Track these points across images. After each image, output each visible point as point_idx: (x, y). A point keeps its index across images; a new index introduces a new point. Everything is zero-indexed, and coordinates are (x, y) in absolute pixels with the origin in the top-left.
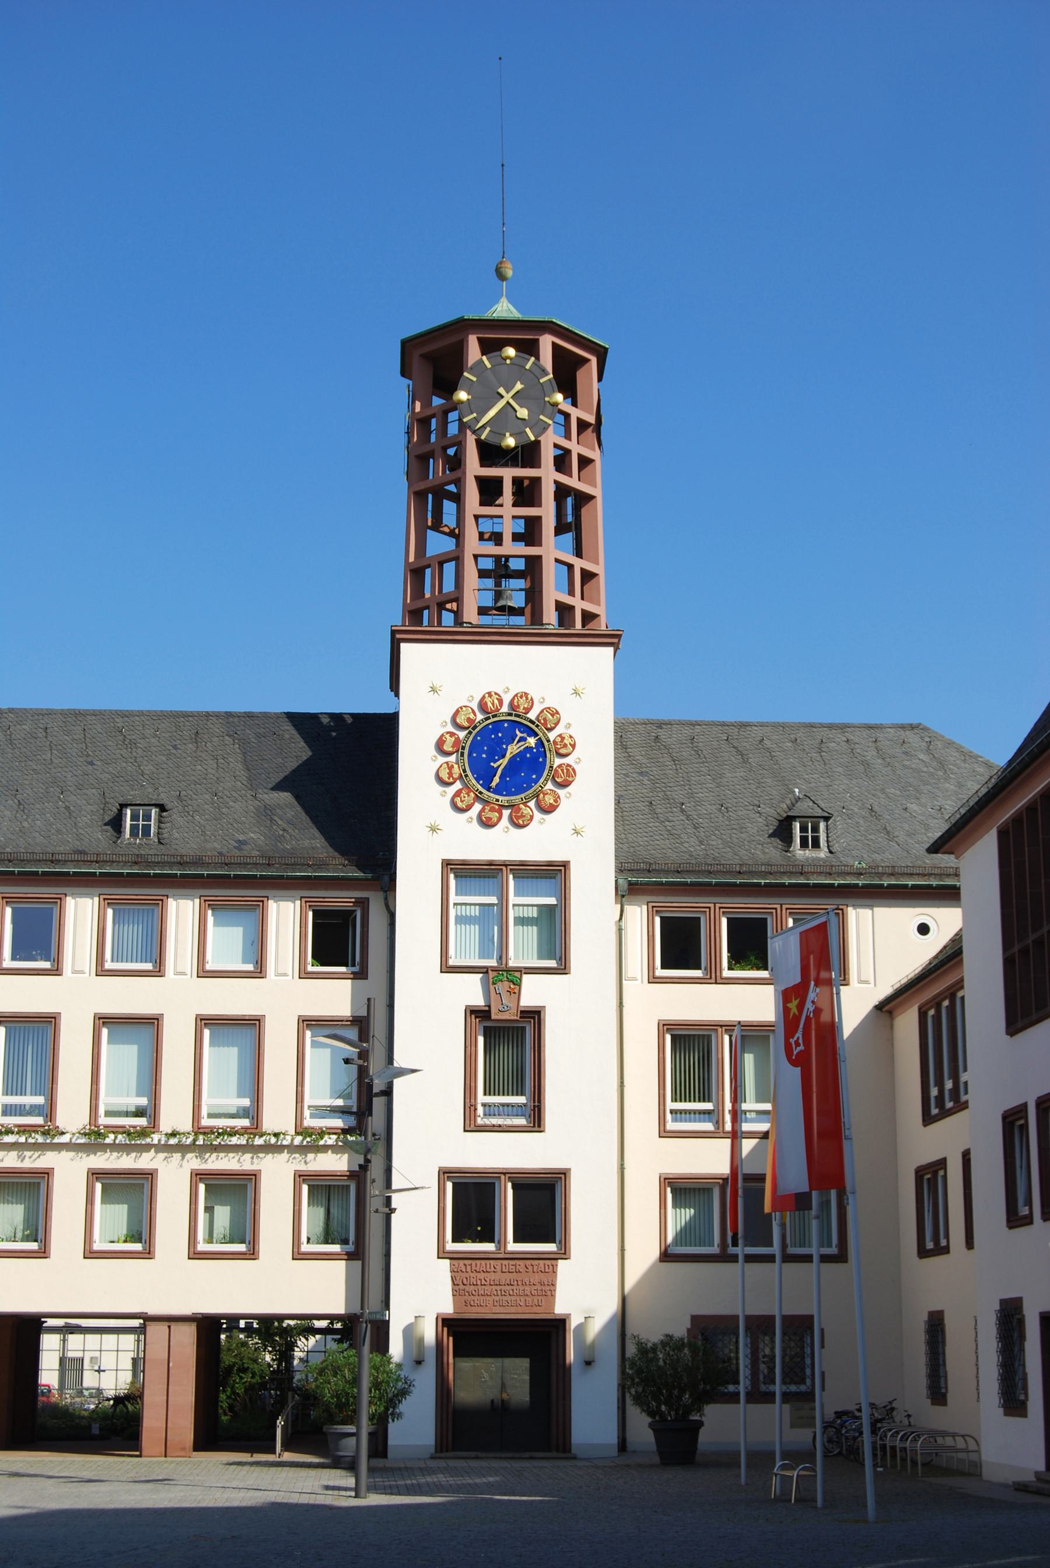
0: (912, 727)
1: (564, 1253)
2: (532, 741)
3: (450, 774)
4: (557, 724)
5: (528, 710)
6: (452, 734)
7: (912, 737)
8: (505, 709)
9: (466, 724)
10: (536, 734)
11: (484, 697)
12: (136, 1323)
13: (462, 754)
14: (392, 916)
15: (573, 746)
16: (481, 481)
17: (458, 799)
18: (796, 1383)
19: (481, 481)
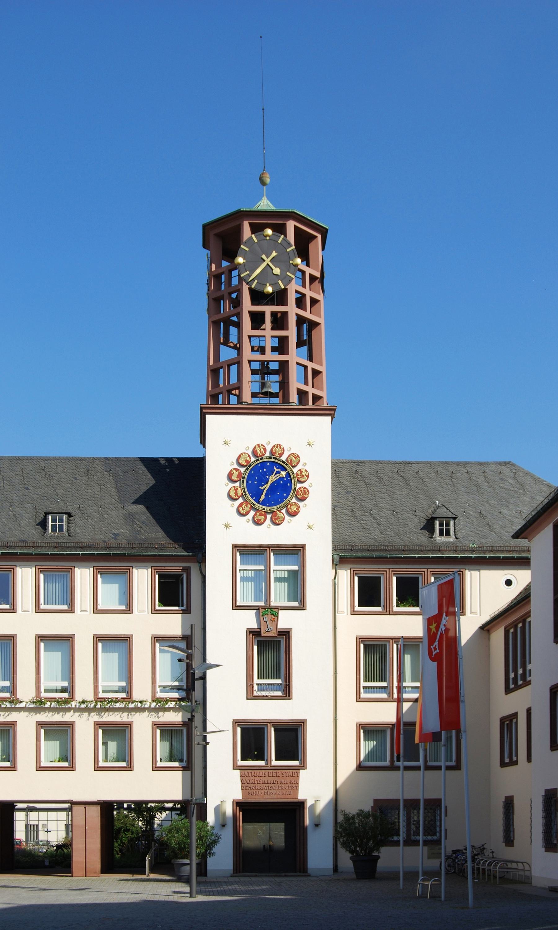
0: (506, 464)
1: (303, 766)
2: (283, 474)
3: (236, 494)
4: (298, 463)
5: (281, 455)
6: (237, 470)
7: (504, 469)
8: (268, 454)
9: (245, 464)
10: (286, 470)
11: (255, 447)
12: (67, 805)
13: (243, 482)
14: (204, 577)
15: (308, 476)
16: (252, 314)
17: (241, 509)
18: (431, 835)
19: (252, 314)
